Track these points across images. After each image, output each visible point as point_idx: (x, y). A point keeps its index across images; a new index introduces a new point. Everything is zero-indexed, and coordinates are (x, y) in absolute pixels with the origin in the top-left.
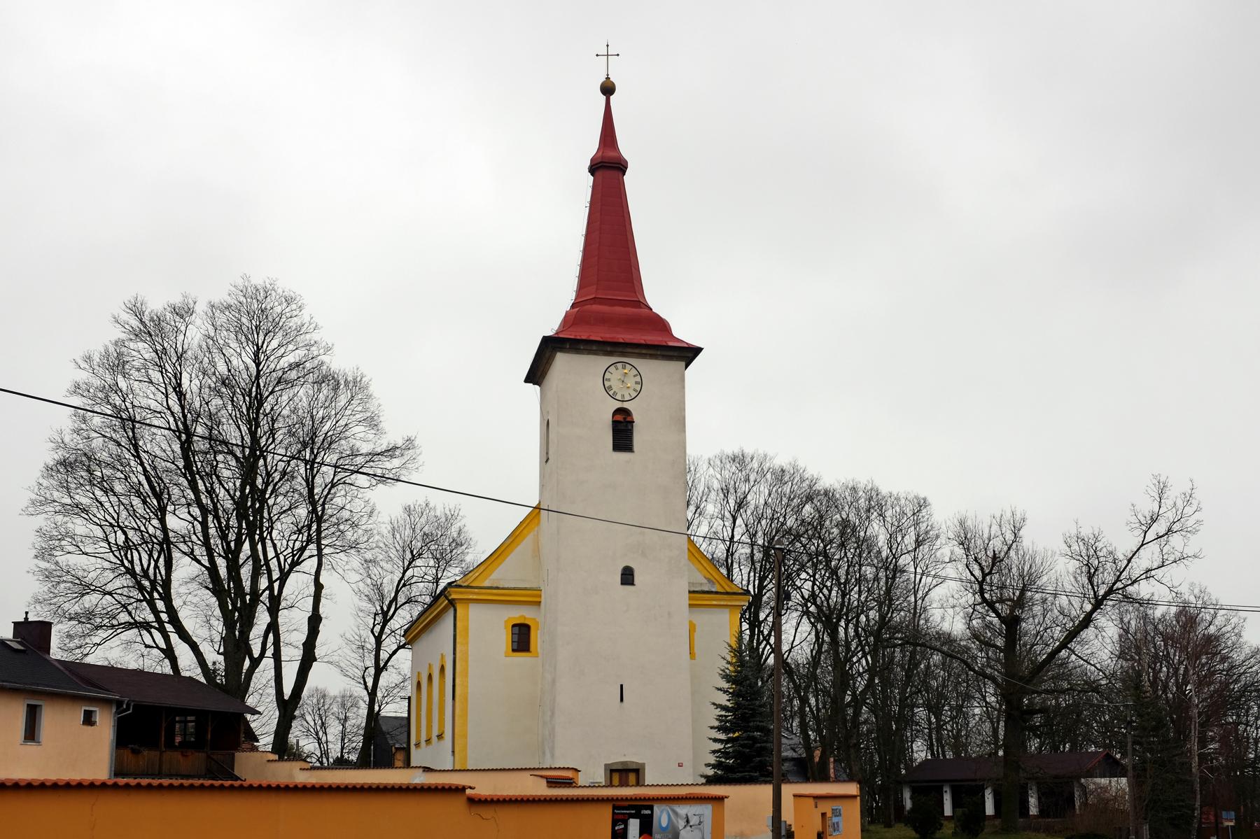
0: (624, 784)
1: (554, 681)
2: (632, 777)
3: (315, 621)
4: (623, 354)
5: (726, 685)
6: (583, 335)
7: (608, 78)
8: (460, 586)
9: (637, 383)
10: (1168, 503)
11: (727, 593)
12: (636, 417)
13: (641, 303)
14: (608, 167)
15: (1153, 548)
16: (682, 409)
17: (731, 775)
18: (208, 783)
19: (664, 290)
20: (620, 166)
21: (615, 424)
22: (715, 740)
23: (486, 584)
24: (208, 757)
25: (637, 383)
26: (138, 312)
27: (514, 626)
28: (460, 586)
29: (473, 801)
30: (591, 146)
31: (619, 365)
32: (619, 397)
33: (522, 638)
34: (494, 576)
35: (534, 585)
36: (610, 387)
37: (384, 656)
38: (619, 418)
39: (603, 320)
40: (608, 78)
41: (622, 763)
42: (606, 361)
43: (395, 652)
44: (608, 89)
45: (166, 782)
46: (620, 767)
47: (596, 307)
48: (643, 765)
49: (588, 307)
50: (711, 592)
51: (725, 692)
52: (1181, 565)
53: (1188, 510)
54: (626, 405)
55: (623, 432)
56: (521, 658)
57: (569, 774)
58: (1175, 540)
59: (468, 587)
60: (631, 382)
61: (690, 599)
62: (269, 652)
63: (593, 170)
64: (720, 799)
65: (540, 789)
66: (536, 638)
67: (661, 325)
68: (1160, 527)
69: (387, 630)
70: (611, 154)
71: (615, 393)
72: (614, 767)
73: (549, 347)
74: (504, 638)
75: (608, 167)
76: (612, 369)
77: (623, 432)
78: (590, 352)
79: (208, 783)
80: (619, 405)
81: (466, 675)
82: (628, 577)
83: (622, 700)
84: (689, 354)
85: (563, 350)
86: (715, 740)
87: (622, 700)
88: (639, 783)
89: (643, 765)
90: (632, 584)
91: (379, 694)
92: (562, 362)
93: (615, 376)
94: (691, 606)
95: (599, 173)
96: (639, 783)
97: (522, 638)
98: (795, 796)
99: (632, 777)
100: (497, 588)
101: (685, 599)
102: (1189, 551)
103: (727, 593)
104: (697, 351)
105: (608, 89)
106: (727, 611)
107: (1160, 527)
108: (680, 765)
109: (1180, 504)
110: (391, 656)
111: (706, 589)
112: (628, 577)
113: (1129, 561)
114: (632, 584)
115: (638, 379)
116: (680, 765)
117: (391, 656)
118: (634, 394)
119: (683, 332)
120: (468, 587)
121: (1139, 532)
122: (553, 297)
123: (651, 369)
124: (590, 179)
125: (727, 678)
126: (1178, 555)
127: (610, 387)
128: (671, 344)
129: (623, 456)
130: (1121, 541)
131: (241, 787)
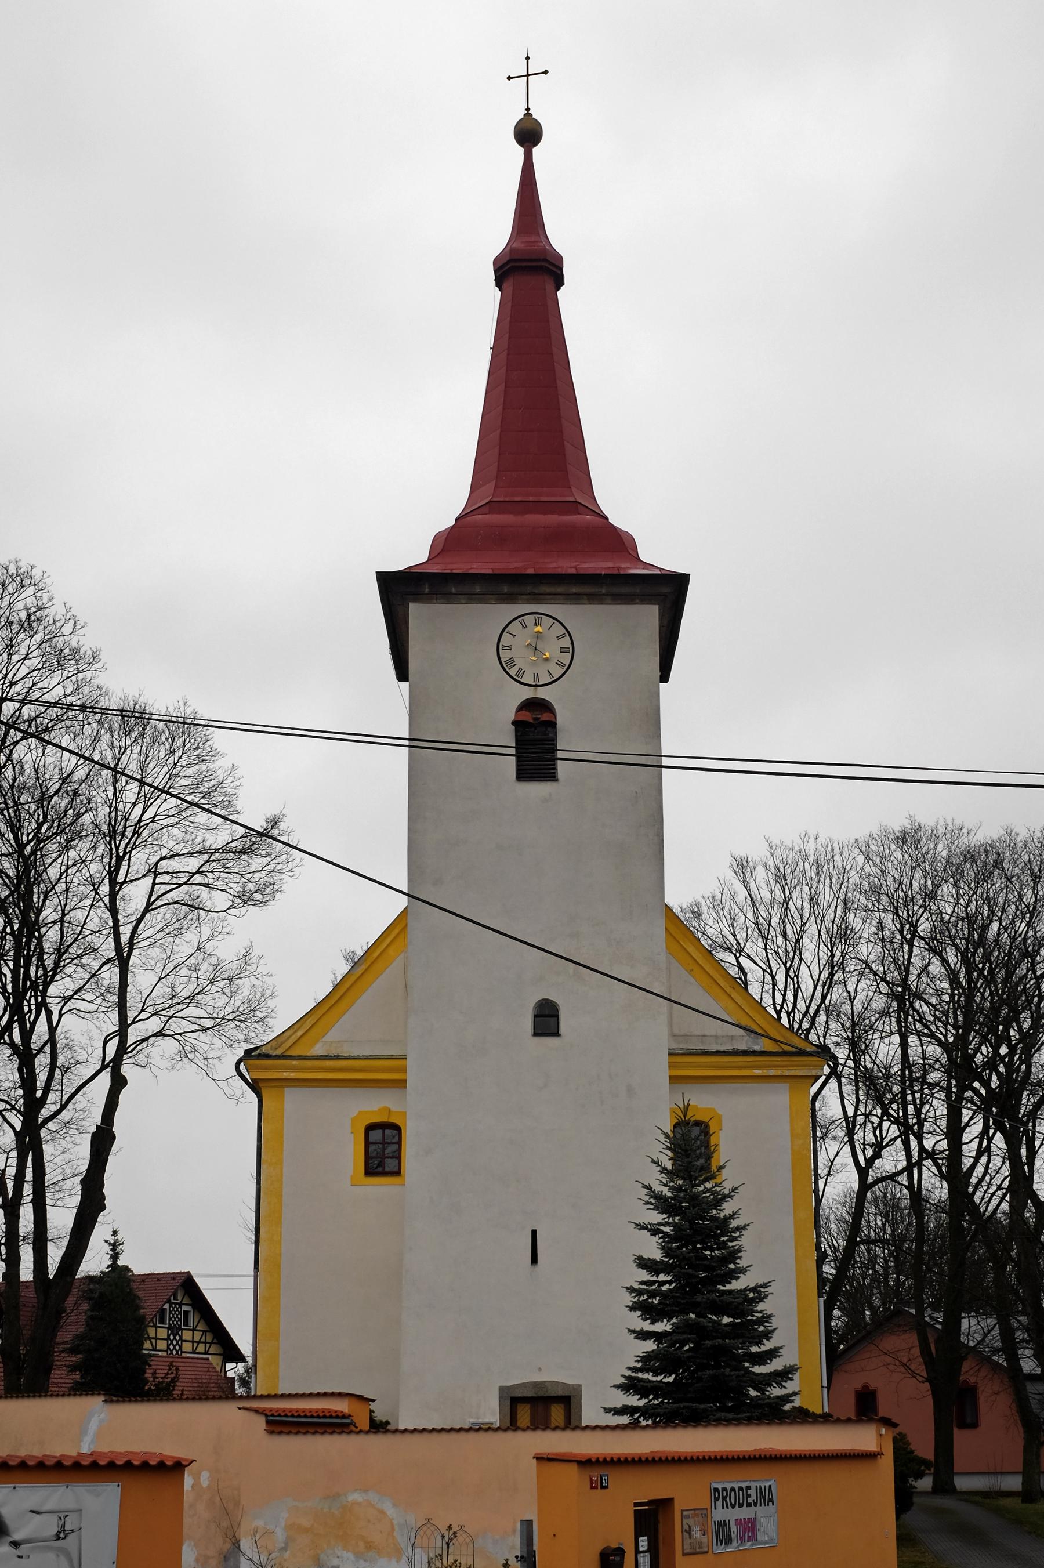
2: (557, 1413)
3: (103, 1141)
5: (656, 1217)
7: (528, 114)
8: (267, 1056)
9: (563, 650)
11: (784, 1054)
12: (562, 718)
14: (529, 271)
19: (636, 480)
22: (643, 1335)
23: (318, 1050)
25: (563, 650)
27: (370, 1128)
28: (267, 1056)
30: (497, 233)
31: (529, 620)
32: (528, 679)
33: (382, 1151)
36: (511, 662)
38: (527, 716)
40: (528, 114)
41: (535, 1385)
44: (528, 134)
46: (530, 1394)
48: (502, 1389)
50: (754, 1053)
51: (654, 1231)
54: (542, 693)
57: (341, 1406)
59: (278, 1057)
60: (551, 650)
61: (671, 1066)
62: (28, 1189)
64: (157, 1472)
67: (621, 544)
71: (521, 672)
72: (519, 1394)
75: (529, 271)
76: (515, 627)
78: (472, 598)
80: (528, 693)
83: (534, 1260)
86: (643, 1335)
87: (534, 1260)
88: (571, 1422)
89: (502, 1389)
90: (557, 1034)
93: (519, 639)
94: (673, 1079)
95: (508, 284)
96: (571, 1422)
97: (382, 1151)
98: (540, 1458)
100: (337, 1057)
105: (528, 134)
106: (784, 1088)
111: (743, 1047)
112: (546, 1019)
114: (557, 1034)
115: (566, 642)
118: (557, 672)
119: (656, 552)
120: (278, 1057)
124: (491, 298)
125: (660, 1203)
127: (511, 662)
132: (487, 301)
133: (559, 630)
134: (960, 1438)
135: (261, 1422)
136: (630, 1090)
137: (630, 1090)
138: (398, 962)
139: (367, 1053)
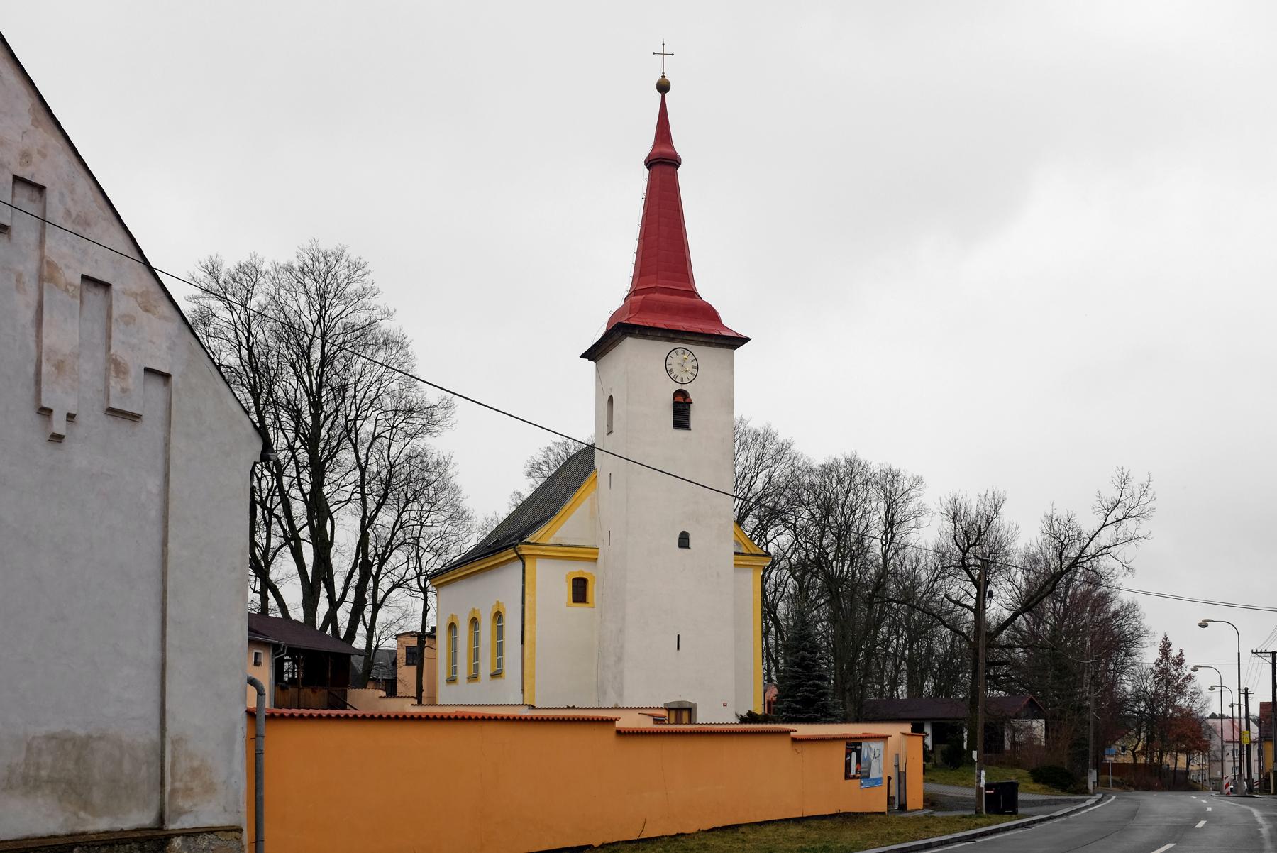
0: (679, 721)
1: (621, 631)
2: (685, 715)
4: (682, 341)
6: (649, 321)
10: (1127, 492)
11: (752, 555)
13: (694, 294)
14: (663, 163)
15: (1111, 529)
16: (732, 393)
17: (799, 716)
18: (324, 713)
19: (710, 281)
20: (674, 162)
21: (676, 405)
23: (551, 541)
24: (329, 693)
26: (213, 272)
29: (795, 740)
30: (646, 144)
33: (580, 590)
34: (557, 535)
35: (591, 544)
37: (381, 595)
38: (680, 399)
39: (665, 309)
42: (667, 346)
43: (390, 591)
44: (663, 87)
45: (306, 712)
47: (657, 296)
48: (695, 704)
49: (651, 296)
52: (1132, 543)
53: (1144, 500)
54: (684, 387)
55: (681, 411)
56: (579, 608)
58: (1130, 523)
63: (650, 163)
65: (648, 724)
66: (593, 591)
67: (710, 314)
68: (1118, 513)
69: (383, 571)
70: (666, 150)
73: (618, 331)
74: (566, 590)
75: (663, 163)
77: (681, 411)
78: (655, 338)
79: (324, 713)
80: (678, 387)
81: (534, 619)
82: (684, 541)
84: (740, 341)
85: (632, 335)
89: (695, 704)
91: (377, 631)
92: (630, 347)
93: (676, 360)
99: (685, 715)
101: (730, 559)
102: (1139, 533)
103: (752, 555)
104: (748, 340)
105: (663, 87)
107: (1118, 513)
108: (725, 705)
109: (1137, 496)
110: (386, 595)
112: (684, 541)
113: (1091, 540)
116: (725, 705)
117: (386, 595)
119: (732, 321)
121: (1103, 516)
122: (610, 281)
123: (704, 353)
126: (1129, 535)
128: (724, 333)
129: (681, 433)
130: (1088, 522)
131: (355, 717)
132: (641, 176)
133: (692, 357)
134: (704, 717)
135: (651, 719)
136: (718, 575)
137: (718, 575)
138: (586, 502)
139: (573, 543)
